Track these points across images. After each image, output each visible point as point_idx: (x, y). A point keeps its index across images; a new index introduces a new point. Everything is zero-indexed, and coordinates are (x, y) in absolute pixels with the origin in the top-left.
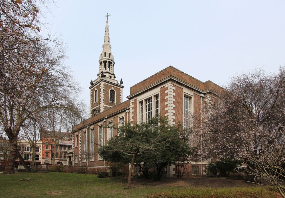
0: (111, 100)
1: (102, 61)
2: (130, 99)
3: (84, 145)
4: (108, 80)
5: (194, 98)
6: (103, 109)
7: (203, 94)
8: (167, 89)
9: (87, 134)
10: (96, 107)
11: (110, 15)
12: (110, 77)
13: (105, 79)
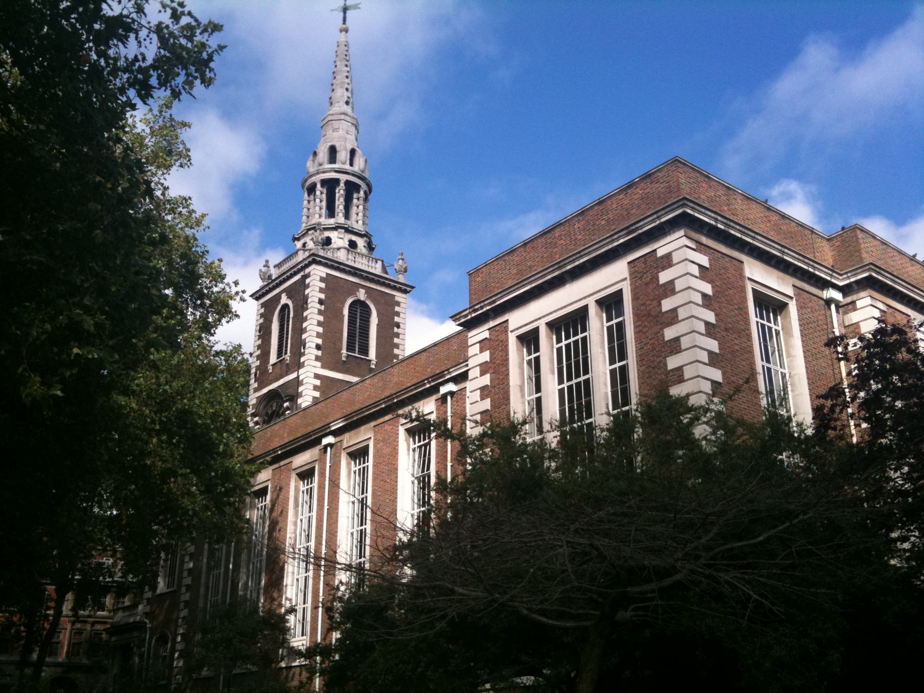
0: (350, 348)
1: (317, 179)
2: (469, 325)
3: (208, 578)
4: (342, 256)
5: (800, 308)
6: (316, 388)
7: (835, 287)
8: (667, 261)
9: (321, 487)
10: (281, 382)
11: (356, 7)
12: (353, 245)
13: (329, 255)
